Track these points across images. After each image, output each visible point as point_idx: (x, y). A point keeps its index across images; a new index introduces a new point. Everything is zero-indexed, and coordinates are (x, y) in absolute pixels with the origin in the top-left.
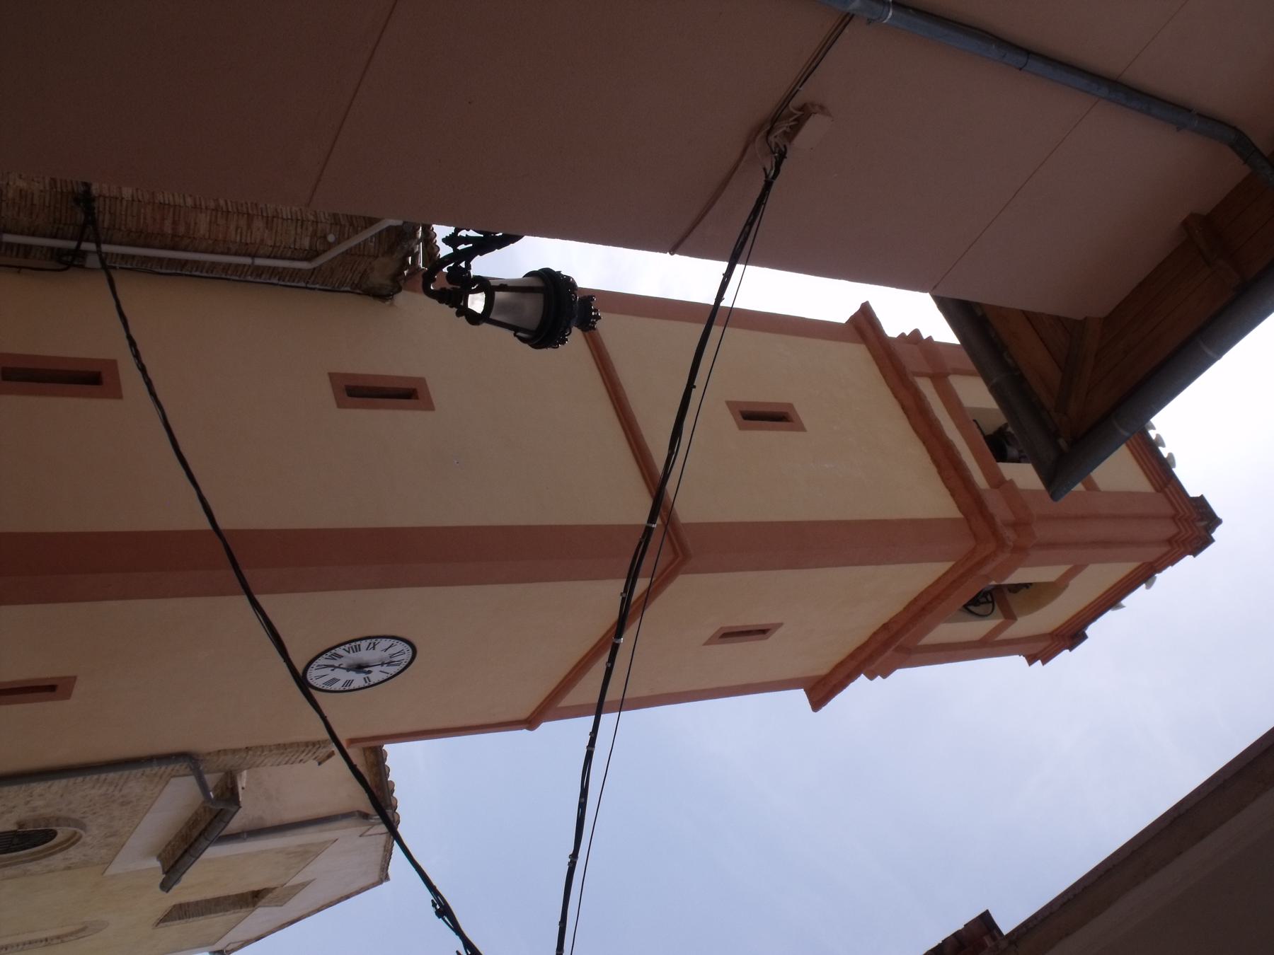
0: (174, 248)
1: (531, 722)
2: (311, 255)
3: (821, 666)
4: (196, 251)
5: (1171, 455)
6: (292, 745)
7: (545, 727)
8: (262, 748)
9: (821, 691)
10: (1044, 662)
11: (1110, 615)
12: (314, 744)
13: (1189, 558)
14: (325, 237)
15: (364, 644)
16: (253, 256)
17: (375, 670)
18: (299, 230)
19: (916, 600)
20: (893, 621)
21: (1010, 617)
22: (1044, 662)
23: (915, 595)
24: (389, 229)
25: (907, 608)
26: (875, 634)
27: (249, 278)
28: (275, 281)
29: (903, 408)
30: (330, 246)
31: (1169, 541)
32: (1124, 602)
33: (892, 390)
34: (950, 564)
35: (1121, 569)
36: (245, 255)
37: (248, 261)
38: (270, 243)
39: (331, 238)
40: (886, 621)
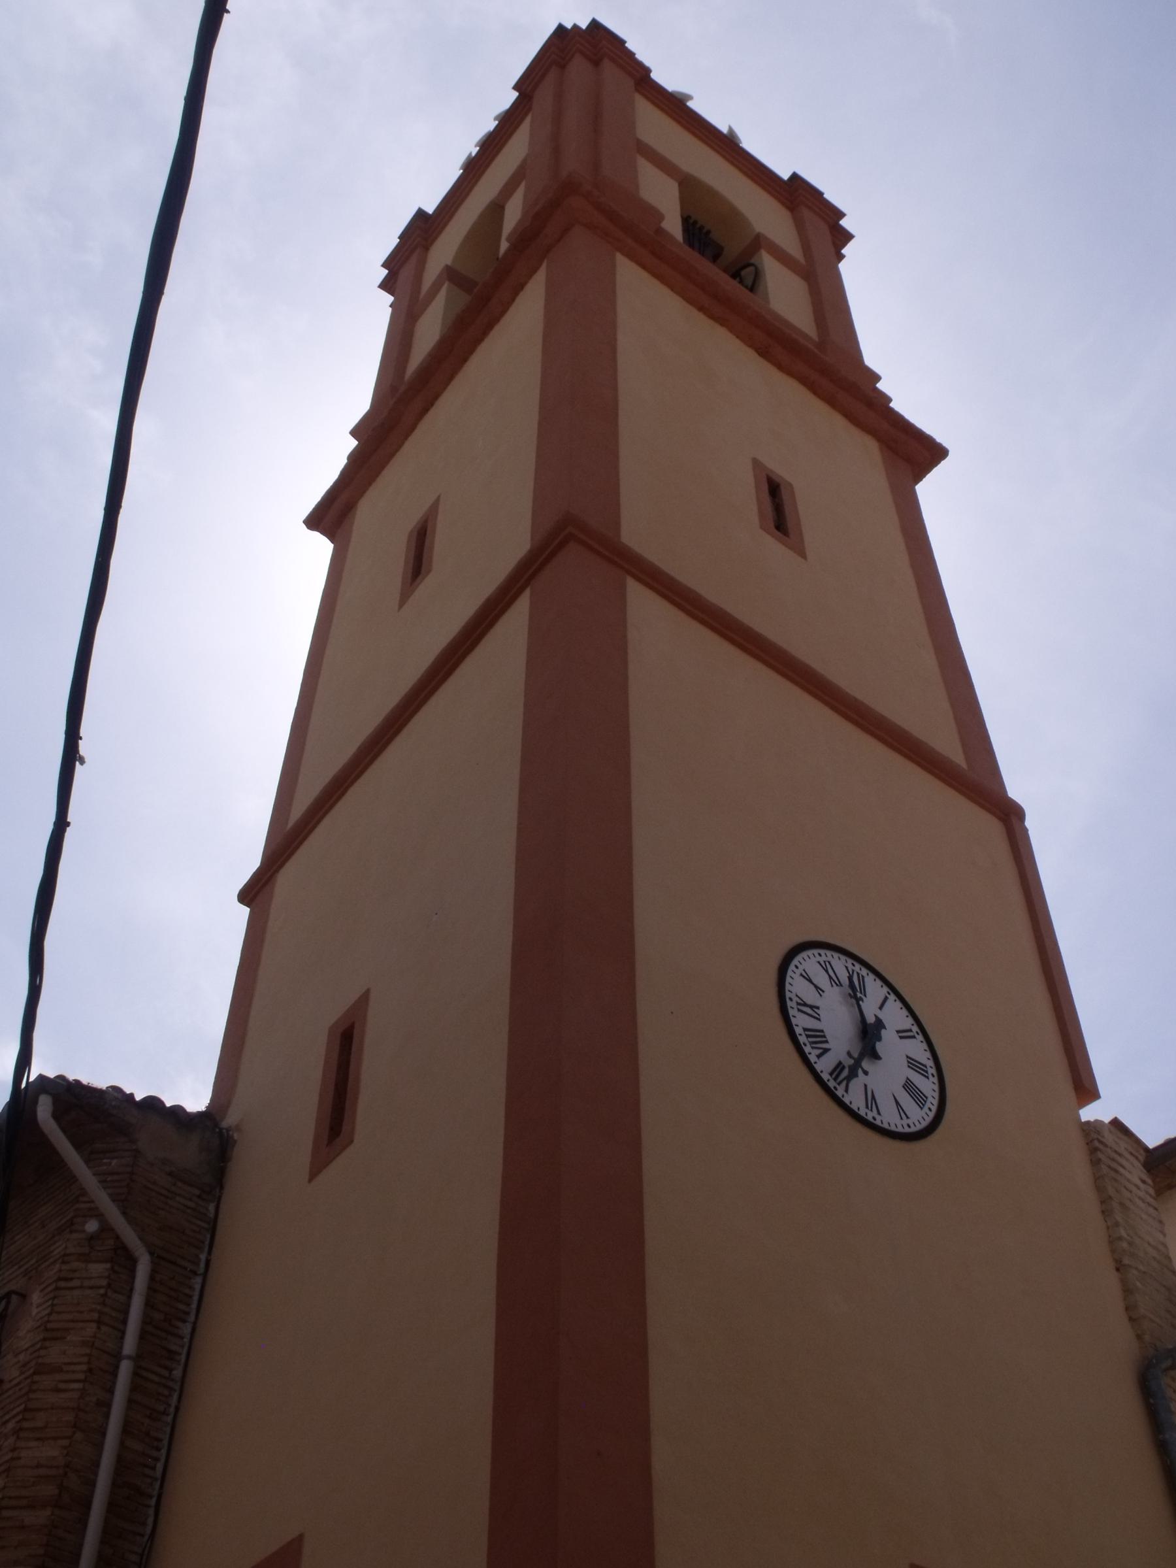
0: (88, 1505)
1: (1010, 816)
2: (123, 1259)
3: (861, 454)
4: (97, 1464)
5: (495, 119)
6: (1099, 1188)
7: (1015, 789)
8: (1113, 1241)
9: (916, 453)
10: (841, 215)
11: (751, 144)
12: (1093, 1151)
13: (653, 75)
14: (92, 1238)
15: (801, 1022)
16: (118, 1357)
17: (870, 1010)
18: (76, 1283)
19: (701, 309)
20: (749, 341)
21: (758, 242)
22: (841, 215)
23: (694, 312)
24: (57, 1116)
25: (722, 321)
26: (780, 367)
27: (177, 1373)
28: (186, 1329)
29: (426, 410)
30: (106, 1228)
31: (596, 63)
32: (725, 130)
33: (407, 436)
34: (620, 258)
35: (644, 110)
36: (115, 1374)
37: (125, 1369)
38: (91, 1329)
39: (92, 1226)
40: (751, 353)
